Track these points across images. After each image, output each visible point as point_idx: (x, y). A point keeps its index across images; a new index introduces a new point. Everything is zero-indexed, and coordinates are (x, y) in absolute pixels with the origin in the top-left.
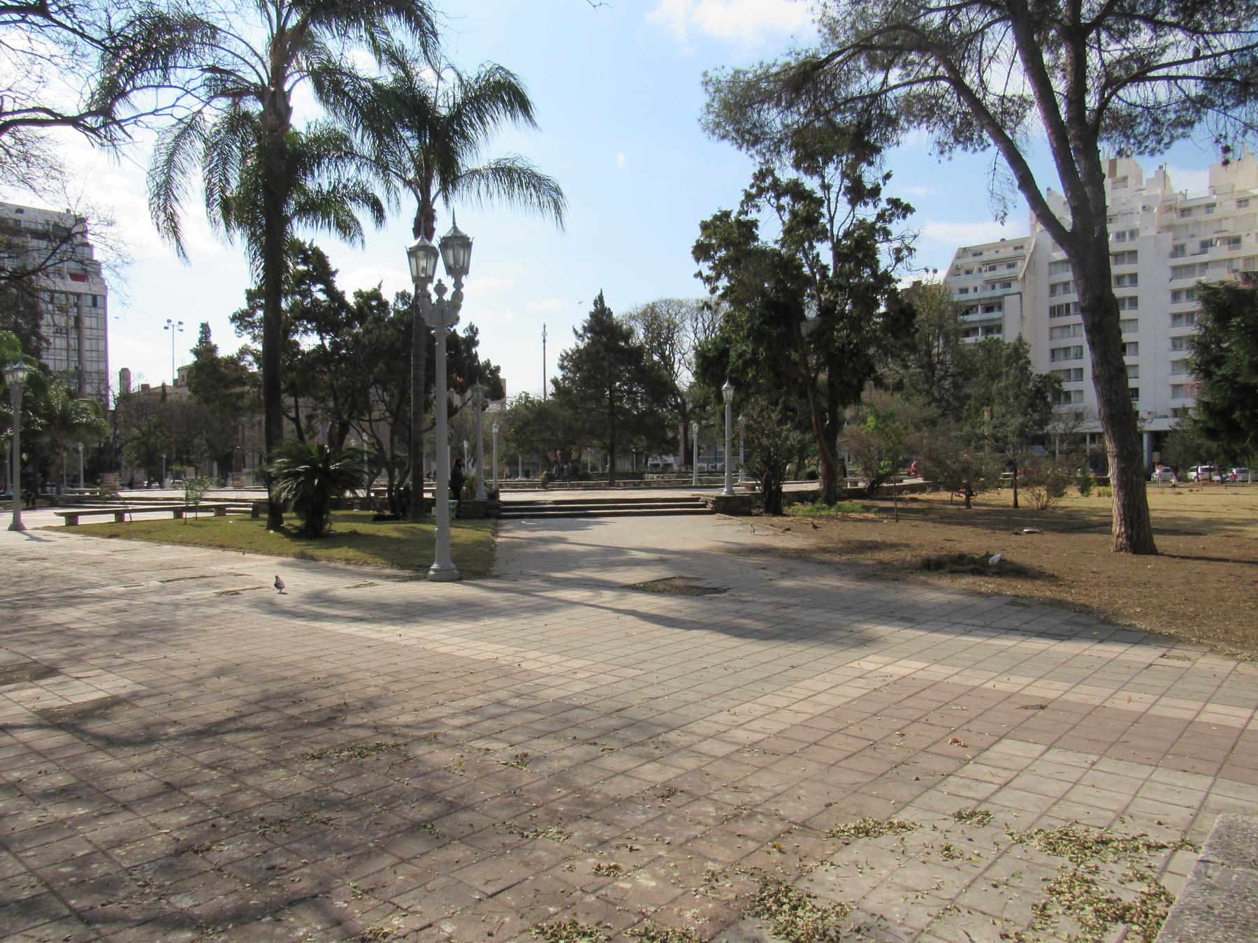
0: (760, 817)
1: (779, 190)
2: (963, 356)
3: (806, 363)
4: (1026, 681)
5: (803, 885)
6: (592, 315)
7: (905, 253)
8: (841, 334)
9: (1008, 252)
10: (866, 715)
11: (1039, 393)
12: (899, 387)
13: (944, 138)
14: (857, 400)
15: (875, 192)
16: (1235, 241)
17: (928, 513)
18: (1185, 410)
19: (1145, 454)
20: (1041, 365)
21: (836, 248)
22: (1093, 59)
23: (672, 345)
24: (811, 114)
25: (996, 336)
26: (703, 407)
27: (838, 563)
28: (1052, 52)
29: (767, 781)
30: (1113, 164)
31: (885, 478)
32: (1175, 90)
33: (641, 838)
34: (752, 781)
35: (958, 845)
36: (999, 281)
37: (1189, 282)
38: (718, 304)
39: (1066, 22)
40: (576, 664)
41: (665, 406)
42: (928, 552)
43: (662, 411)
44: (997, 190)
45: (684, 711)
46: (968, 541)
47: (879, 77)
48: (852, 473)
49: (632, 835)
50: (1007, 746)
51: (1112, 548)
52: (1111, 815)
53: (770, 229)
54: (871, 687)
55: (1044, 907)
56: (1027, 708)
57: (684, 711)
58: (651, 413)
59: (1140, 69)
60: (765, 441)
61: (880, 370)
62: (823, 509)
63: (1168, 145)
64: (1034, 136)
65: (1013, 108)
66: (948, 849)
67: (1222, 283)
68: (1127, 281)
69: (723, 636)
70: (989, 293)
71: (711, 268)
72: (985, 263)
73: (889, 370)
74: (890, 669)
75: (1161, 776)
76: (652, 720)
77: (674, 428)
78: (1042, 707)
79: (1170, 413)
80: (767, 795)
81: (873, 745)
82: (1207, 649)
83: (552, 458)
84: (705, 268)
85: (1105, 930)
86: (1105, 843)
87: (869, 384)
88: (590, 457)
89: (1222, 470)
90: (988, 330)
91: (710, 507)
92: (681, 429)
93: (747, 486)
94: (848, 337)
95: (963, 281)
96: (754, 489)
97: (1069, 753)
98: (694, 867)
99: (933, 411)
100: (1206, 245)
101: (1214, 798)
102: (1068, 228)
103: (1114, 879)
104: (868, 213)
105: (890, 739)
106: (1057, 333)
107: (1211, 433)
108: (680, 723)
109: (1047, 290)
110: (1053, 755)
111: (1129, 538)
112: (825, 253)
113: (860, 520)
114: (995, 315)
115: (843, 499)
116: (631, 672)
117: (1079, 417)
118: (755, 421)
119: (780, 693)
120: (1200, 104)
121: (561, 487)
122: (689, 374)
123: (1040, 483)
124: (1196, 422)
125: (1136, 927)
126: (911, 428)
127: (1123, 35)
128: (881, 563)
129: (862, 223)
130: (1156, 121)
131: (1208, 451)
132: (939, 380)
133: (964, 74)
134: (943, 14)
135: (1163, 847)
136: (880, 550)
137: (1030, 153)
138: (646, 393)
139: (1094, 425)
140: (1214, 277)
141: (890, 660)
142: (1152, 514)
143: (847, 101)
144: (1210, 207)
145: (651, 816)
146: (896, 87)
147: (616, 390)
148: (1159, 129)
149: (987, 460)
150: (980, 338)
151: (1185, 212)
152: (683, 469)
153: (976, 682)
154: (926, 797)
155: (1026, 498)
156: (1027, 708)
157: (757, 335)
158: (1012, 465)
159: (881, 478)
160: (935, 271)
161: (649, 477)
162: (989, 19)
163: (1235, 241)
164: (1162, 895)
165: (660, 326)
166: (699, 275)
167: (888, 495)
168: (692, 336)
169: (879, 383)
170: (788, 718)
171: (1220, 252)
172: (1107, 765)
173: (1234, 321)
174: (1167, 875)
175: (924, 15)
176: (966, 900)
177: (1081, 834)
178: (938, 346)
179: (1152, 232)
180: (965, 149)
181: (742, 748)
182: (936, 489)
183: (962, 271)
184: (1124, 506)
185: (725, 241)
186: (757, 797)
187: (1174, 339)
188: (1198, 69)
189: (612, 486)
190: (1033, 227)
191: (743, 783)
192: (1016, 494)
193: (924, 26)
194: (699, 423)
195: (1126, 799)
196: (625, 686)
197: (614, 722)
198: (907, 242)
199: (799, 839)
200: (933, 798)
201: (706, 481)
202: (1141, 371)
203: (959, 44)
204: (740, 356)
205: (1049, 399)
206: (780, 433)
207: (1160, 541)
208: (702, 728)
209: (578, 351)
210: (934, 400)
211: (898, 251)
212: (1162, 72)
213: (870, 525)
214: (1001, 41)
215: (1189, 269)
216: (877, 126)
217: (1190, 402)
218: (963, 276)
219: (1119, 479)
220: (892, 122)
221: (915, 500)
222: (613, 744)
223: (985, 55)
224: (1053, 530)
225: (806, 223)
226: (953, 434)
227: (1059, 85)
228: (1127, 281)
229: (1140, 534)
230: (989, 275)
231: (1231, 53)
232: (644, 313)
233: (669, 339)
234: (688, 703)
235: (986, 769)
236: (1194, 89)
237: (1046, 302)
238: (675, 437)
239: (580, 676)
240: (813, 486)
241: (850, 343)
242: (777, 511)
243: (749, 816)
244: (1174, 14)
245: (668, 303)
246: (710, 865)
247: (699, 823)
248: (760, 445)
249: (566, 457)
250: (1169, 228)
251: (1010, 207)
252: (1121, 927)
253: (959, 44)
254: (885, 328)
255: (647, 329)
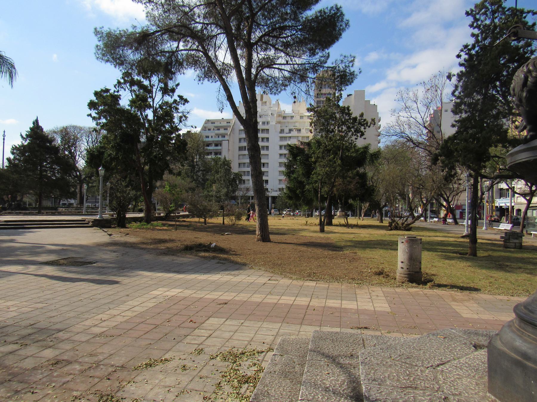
0: (102, 366)
1: (133, 83)
2: (206, 163)
3: (140, 161)
4: (220, 293)
5: (119, 394)
6: (31, 129)
7: (184, 118)
8: (156, 151)
9: (225, 124)
10: (154, 314)
11: (234, 180)
12: (179, 174)
13: (200, 75)
14: (161, 179)
15: (173, 91)
16: (299, 130)
17: (189, 227)
18: (283, 189)
19: (270, 205)
20: (235, 169)
21: (155, 112)
22: (255, 56)
23: (75, 147)
24: (143, 54)
25: (219, 156)
26: (90, 177)
27: (149, 249)
28: (241, 50)
29: (107, 350)
30: (262, 97)
31: (173, 211)
32: (281, 74)
33: (39, 386)
34: (100, 350)
35: (189, 364)
36: (221, 134)
37: (285, 143)
38: (100, 130)
39: (246, 40)
40: (9, 303)
41: (71, 176)
42: (188, 243)
43: (70, 179)
44: (220, 99)
45: (68, 322)
46: (204, 238)
47: (175, 44)
48: (159, 209)
49: (34, 386)
50: (212, 321)
51: (256, 240)
52: (246, 342)
53: (125, 99)
54: (158, 302)
55: (220, 383)
56: (220, 304)
57: (68, 322)
58: (62, 178)
59: (269, 63)
60: (119, 195)
61: (172, 166)
62: (144, 225)
63: (280, 92)
64: (233, 80)
65: (226, 68)
66: (184, 367)
67: (295, 145)
68: (265, 140)
69: (92, 284)
70: (217, 139)
71: (96, 113)
72: (216, 127)
73: (176, 167)
74: (167, 293)
75: (265, 325)
76: (50, 328)
77: (75, 186)
78: (226, 304)
79: (278, 190)
80: (106, 356)
81: (157, 326)
82: (283, 276)
83: (6, 199)
84: (94, 113)
85: (241, 387)
86: (243, 354)
87: (166, 172)
88: (28, 199)
89: (294, 211)
90: (216, 154)
91: (90, 224)
92: (78, 187)
93: (110, 215)
94: (158, 151)
95: (207, 133)
96: (113, 216)
97: (234, 321)
98: (66, 395)
99: (193, 185)
100: (290, 130)
101: (281, 331)
102: (244, 118)
103: (246, 368)
104: (168, 99)
105: (164, 324)
106: (241, 157)
107: (290, 198)
108: (65, 327)
109: (238, 140)
110: (228, 322)
111: (261, 236)
112: (150, 114)
113: (161, 230)
114: (219, 148)
115: (154, 221)
116: (40, 305)
117: (248, 190)
118: (114, 185)
119: (117, 308)
120: (289, 79)
121: (10, 214)
122: (84, 162)
123: (233, 215)
124: (285, 193)
125: (251, 384)
126: (184, 191)
127: (266, 50)
128: (168, 248)
129: (167, 103)
130: (276, 83)
131: (289, 204)
132: (196, 172)
133: (209, 51)
134: (201, 25)
135: (263, 352)
136: (168, 242)
137: (232, 87)
138: (60, 169)
139: (251, 193)
140: (293, 142)
141: (168, 289)
142: (270, 227)
143: (161, 52)
144: (292, 117)
145: (45, 375)
146: (182, 50)
147: (44, 166)
148: (275, 86)
149: (215, 206)
150: (213, 156)
151: (284, 118)
152: (79, 206)
153: (202, 296)
154: (177, 346)
155: (227, 221)
156: (220, 304)
157: (118, 148)
158: (222, 208)
159: (170, 212)
160: (196, 127)
161: (60, 209)
162: (219, 31)
163: (299, 130)
164: (261, 370)
165: (69, 138)
166: (90, 115)
167: (173, 219)
168: (86, 144)
169: (171, 172)
170: (120, 319)
171: (294, 133)
172: (247, 323)
173: (298, 158)
174: (264, 362)
175: (194, 24)
176: (190, 387)
177: (235, 352)
178: (197, 159)
179: (274, 123)
180: (209, 80)
181: (96, 336)
182: (193, 217)
183: (207, 129)
184: (260, 224)
185: (104, 102)
186: (101, 357)
187: (280, 163)
188: (288, 68)
189: (39, 213)
190: (233, 116)
191: (95, 352)
192: (224, 219)
193: (194, 28)
194: (88, 185)
195: (252, 335)
196: (37, 312)
197: (30, 331)
198: (185, 114)
199: (120, 373)
200: (181, 346)
201: (90, 212)
202: (269, 174)
203: (208, 38)
204: (109, 155)
205: (237, 182)
206: (126, 191)
207: (272, 237)
208: (79, 328)
209: (23, 146)
210: (194, 180)
211: (181, 117)
212: (277, 66)
213: (164, 232)
214: (222, 40)
215: (285, 138)
216: (174, 65)
217: (284, 187)
218: (207, 131)
219: (259, 214)
220: (181, 64)
221: (185, 221)
222: (28, 342)
223: (217, 46)
224: (236, 233)
225: (141, 102)
226: (200, 195)
227: (243, 63)
228: (265, 140)
229: (265, 235)
230: (217, 132)
231: (298, 64)
232: (61, 131)
233: (74, 144)
234: (69, 318)
235: (202, 331)
236: (287, 74)
237: (237, 145)
238: (75, 191)
239: (11, 309)
240: (141, 215)
241: (160, 154)
242: (123, 226)
243: (97, 367)
244: (281, 46)
245: (75, 127)
246: (75, 393)
247: (71, 374)
248: (116, 196)
249: (14, 199)
250: (279, 122)
251: (225, 106)
252: (247, 385)
253: (208, 38)
254: (175, 149)
255: (62, 139)
